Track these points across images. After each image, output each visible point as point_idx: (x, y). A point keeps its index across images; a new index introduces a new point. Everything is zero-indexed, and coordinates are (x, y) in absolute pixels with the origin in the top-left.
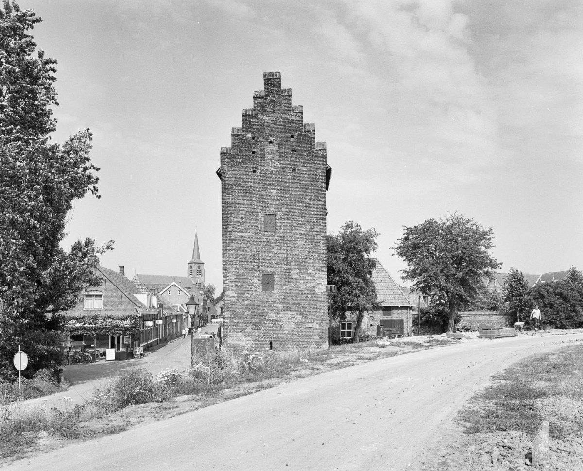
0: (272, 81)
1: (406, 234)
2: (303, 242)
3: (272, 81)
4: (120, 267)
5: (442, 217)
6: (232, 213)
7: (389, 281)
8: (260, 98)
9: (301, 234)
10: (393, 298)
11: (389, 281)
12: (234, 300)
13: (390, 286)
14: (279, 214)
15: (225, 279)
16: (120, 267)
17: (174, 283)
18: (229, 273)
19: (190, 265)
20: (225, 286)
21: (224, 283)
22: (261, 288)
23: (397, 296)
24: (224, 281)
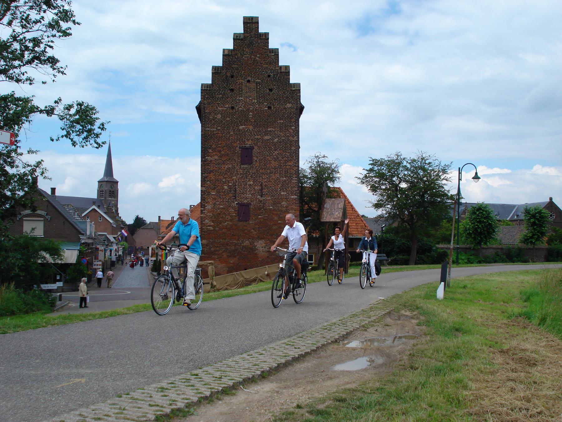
0: (251, 23)
1: (371, 164)
2: (277, 175)
3: (251, 23)
4: (52, 189)
5: (409, 152)
6: (211, 146)
7: (352, 212)
8: (239, 39)
9: (275, 168)
10: (356, 230)
11: (352, 212)
12: (211, 228)
13: (353, 217)
14: (256, 148)
15: (202, 209)
16: (52, 189)
17: (94, 207)
18: (207, 203)
19: (101, 183)
20: (202, 215)
21: (202, 213)
22: (237, 218)
23: (359, 227)
24: (202, 211)
